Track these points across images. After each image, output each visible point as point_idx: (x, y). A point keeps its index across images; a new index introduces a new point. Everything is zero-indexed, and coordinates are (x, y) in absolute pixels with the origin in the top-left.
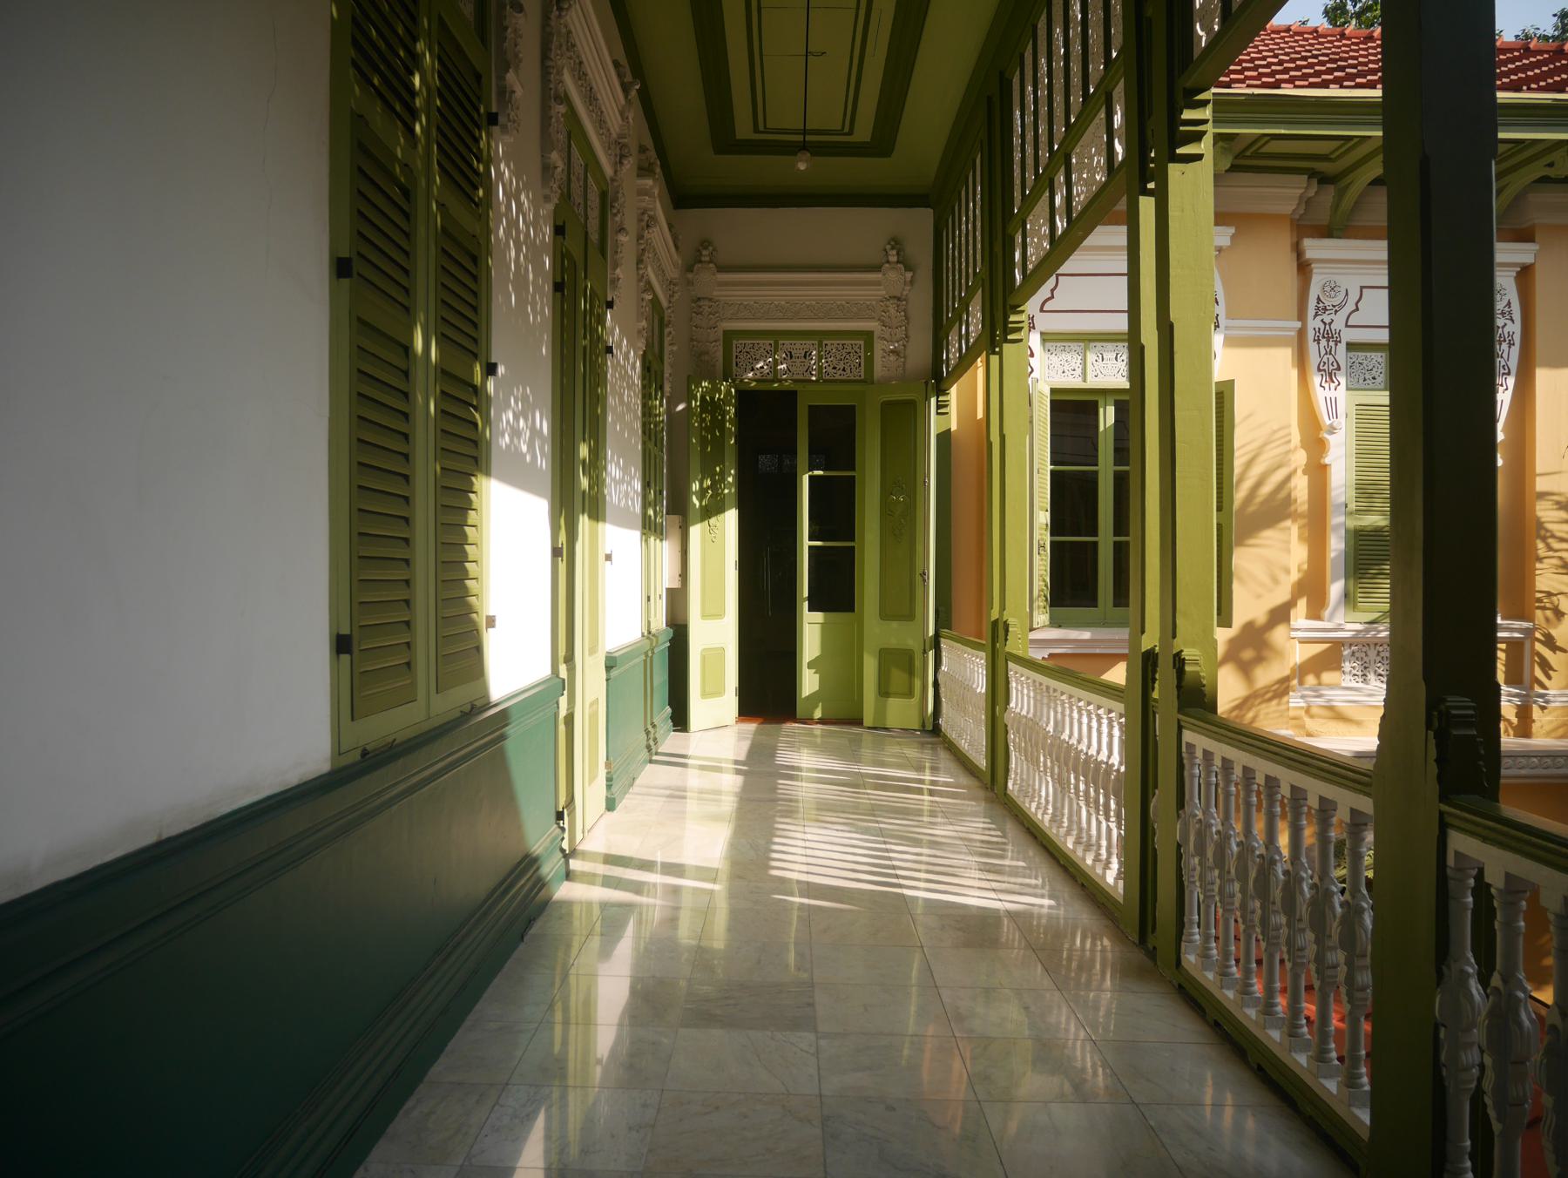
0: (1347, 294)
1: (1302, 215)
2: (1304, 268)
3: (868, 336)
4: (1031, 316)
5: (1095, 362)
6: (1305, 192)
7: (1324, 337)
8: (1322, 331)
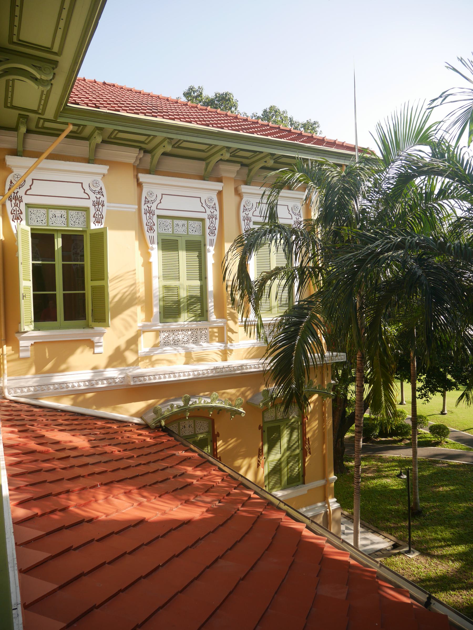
0: (157, 196)
1: (138, 164)
2: (139, 185)
3: (202, 220)
4: (21, 196)
5: (51, 218)
6: (138, 155)
7: (148, 212)
8: (147, 210)
